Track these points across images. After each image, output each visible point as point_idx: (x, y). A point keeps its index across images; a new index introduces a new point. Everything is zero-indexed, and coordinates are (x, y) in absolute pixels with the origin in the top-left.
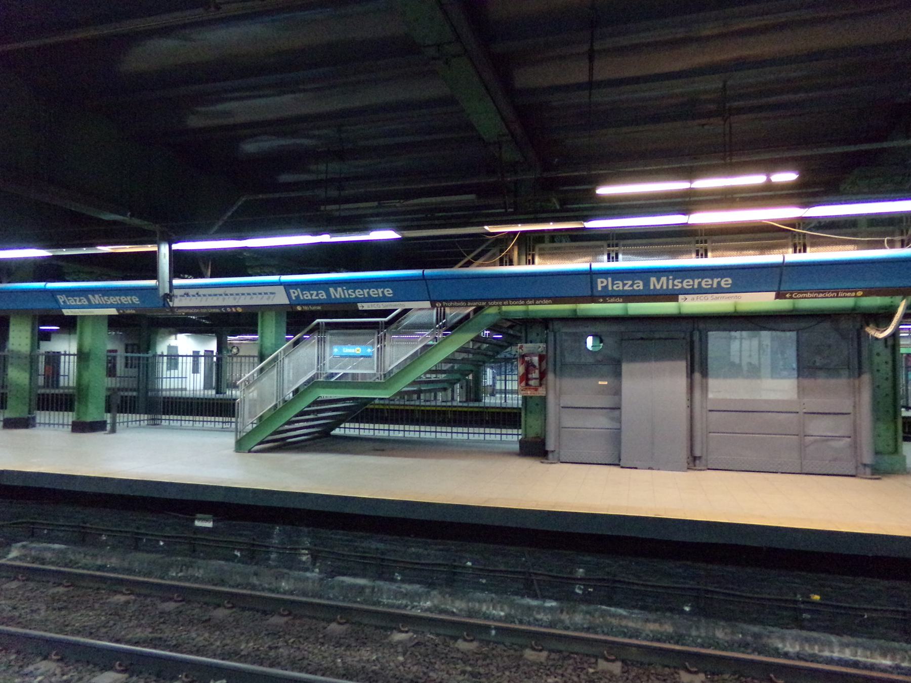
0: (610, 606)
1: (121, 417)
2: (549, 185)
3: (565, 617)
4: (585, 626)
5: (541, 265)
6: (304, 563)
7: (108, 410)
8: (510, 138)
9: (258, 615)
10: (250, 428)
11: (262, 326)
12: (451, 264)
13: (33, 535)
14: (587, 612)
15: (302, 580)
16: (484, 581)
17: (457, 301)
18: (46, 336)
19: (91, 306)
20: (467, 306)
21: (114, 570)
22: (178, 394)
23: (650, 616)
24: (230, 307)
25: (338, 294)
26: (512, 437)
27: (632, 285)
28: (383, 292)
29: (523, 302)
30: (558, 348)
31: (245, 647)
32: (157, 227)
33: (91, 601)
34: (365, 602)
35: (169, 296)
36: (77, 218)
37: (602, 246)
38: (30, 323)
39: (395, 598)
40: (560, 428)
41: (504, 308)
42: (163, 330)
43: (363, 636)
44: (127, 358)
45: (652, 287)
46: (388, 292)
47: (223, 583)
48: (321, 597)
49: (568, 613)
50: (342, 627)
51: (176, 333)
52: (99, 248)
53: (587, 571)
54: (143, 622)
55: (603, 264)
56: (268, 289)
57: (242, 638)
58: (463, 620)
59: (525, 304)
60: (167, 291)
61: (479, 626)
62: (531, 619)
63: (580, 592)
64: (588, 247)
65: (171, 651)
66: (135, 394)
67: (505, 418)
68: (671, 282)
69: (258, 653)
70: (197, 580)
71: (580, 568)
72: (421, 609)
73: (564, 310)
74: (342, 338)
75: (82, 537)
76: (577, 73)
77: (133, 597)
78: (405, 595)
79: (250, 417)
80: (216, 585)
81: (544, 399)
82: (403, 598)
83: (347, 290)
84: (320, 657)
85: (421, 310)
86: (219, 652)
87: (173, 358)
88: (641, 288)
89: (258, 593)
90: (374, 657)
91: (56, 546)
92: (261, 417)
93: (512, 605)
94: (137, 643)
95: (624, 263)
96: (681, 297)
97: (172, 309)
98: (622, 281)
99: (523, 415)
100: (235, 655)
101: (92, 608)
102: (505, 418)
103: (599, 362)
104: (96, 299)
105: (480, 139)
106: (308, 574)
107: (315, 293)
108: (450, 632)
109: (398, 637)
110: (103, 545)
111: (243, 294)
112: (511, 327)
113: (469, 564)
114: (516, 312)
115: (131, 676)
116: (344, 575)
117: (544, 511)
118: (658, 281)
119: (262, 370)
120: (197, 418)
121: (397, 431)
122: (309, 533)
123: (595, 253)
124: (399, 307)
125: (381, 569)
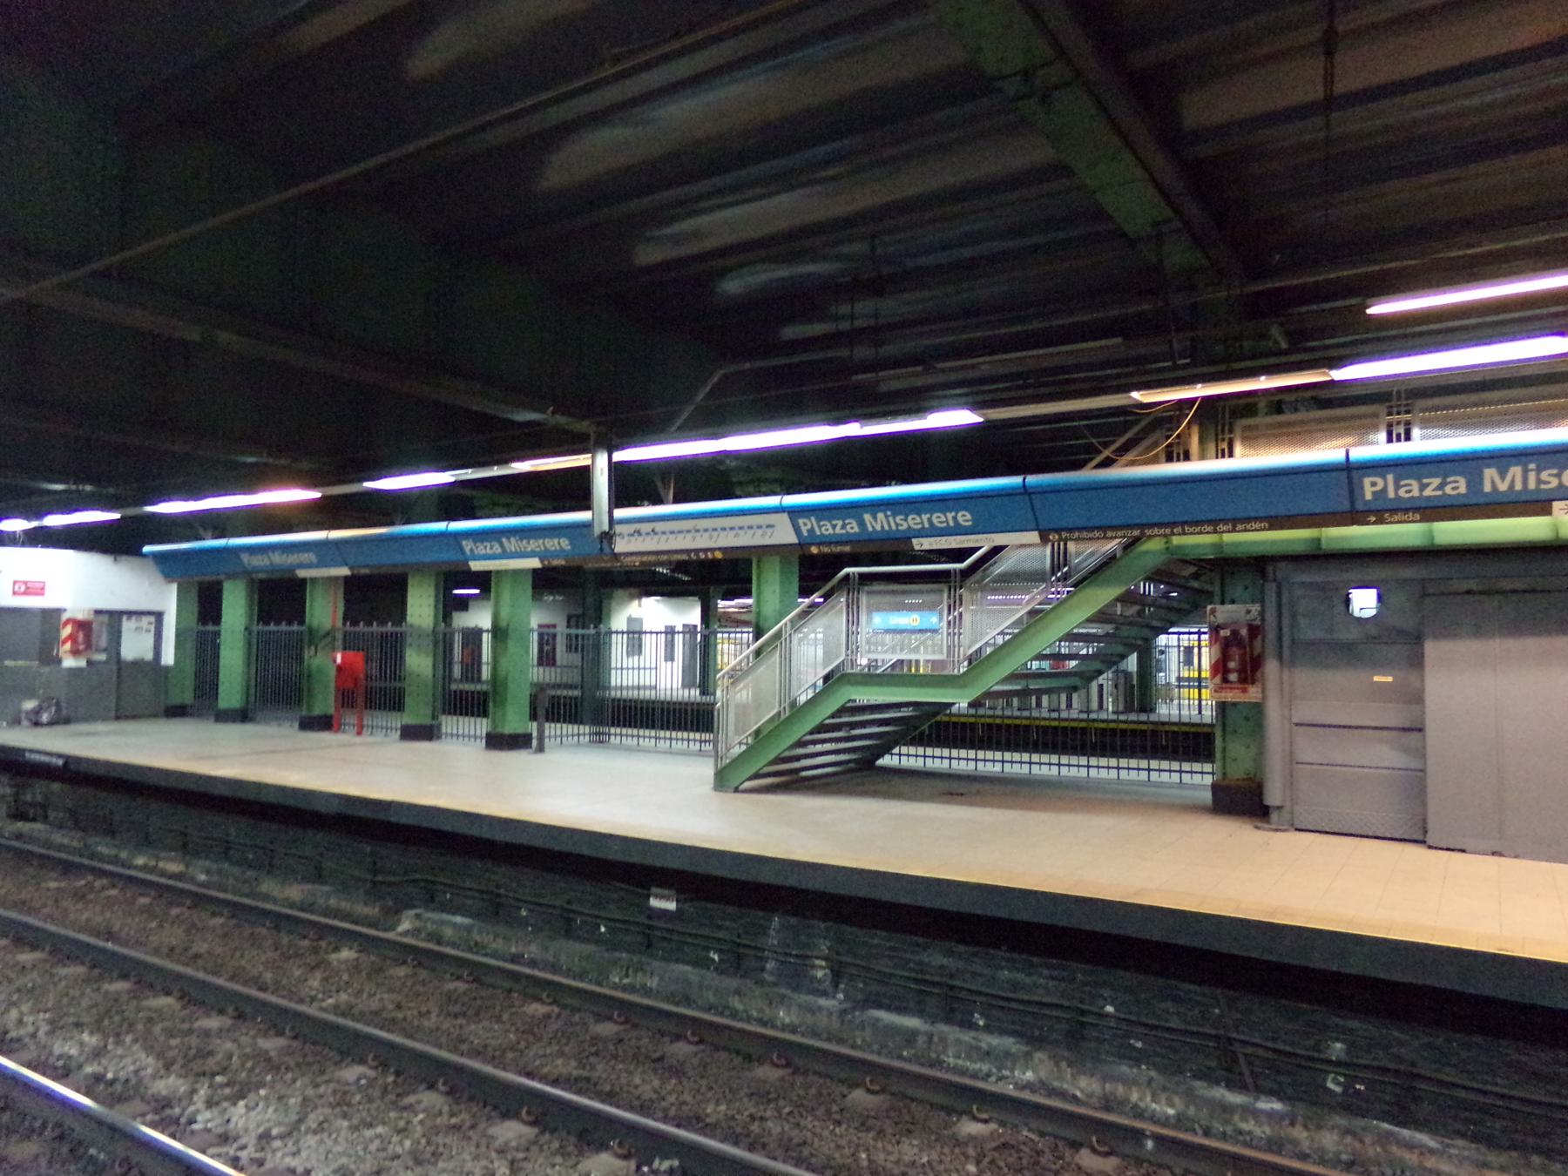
0: (1404, 1125)
1: (551, 729)
2: (1274, 304)
3: (1299, 1133)
4: (1344, 1157)
5: (1245, 459)
6: (819, 981)
7: (534, 716)
8: (1177, 224)
9: (738, 1060)
10: (737, 750)
11: (759, 585)
12: (1078, 465)
13: (431, 899)
14: (1347, 1132)
15: (810, 1011)
16: (1139, 1045)
17: (1091, 529)
18: (463, 604)
19: (505, 555)
20: (1105, 538)
21: (533, 963)
22: (647, 695)
23: (1492, 1157)
24: (705, 550)
25: (878, 523)
26: (1199, 778)
27: (1441, 487)
28: (955, 518)
29: (1210, 528)
30: (1285, 611)
31: (715, 1110)
32: (584, 426)
33: (498, 1008)
34: (915, 1058)
35: (608, 537)
36: (486, 423)
37: (1376, 415)
38: (433, 584)
39: (969, 1057)
40: (1292, 762)
41: (1177, 540)
42: (619, 593)
43: (907, 1118)
44: (569, 636)
45: (1487, 488)
46: (965, 518)
47: (687, 1001)
48: (841, 1041)
49: (1306, 1127)
50: (870, 1097)
51: (640, 596)
52: (514, 465)
53: (1351, 1046)
54: (567, 1049)
55: (1377, 447)
56: (761, 520)
57: (710, 1094)
58: (1091, 1113)
59: (1215, 532)
60: (606, 528)
61: (1126, 1129)
62: (1229, 1130)
63: (1338, 1089)
64: (1353, 417)
65: (603, 1101)
66: (577, 693)
67: (1189, 743)
68: (1532, 476)
69: (733, 1124)
70: (648, 992)
71: (1338, 1040)
72: (1016, 1084)
73: (1293, 541)
74: (888, 599)
75: (495, 910)
76: (1301, 83)
77: (556, 1009)
78: (987, 1055)
79: (737, 732)
80: (677, 1004)
81: (1258, 709)
82: (982, 1060)
83: (894, 515)
84: (832, 1145)
85: (1024, 548)
86: (672, 1112)
87: (635, 635)
88: (1463, 490)
89: (739, 1025)
90: (925, 1160)
91: (458, 919)
92: (757, 732)
93: (1190, 1096)
94: (555, 1083)
95: (1424, 443)
96: (1556, 505)
97: (616, 556)
98: (1419, 479)
99: (1218, 742)
100: (695, 1121)
101: (498, 1019)
102: (1189, 743)
103: (1372, 639)
104: (512, 544)
105: (1124, 235)
106: (822, 1002)
107: (840, 523)
108: (1072, 1134)
109: (970, 1128)
110: (524, 923)
111: (724, 529)
112: (1196, 576)
113: (1110, 1009)
114: (1198, 546)
115: (542, 1132)
116: (879, 1006)
117: (1248, 921)
118: (1503, 476)
119: (758, 653)
120: (662, 734)
121: (990, 762)
122: (827, 929)
123: (1362, 428)
124: (985, 543)
125: (952, 1005)
